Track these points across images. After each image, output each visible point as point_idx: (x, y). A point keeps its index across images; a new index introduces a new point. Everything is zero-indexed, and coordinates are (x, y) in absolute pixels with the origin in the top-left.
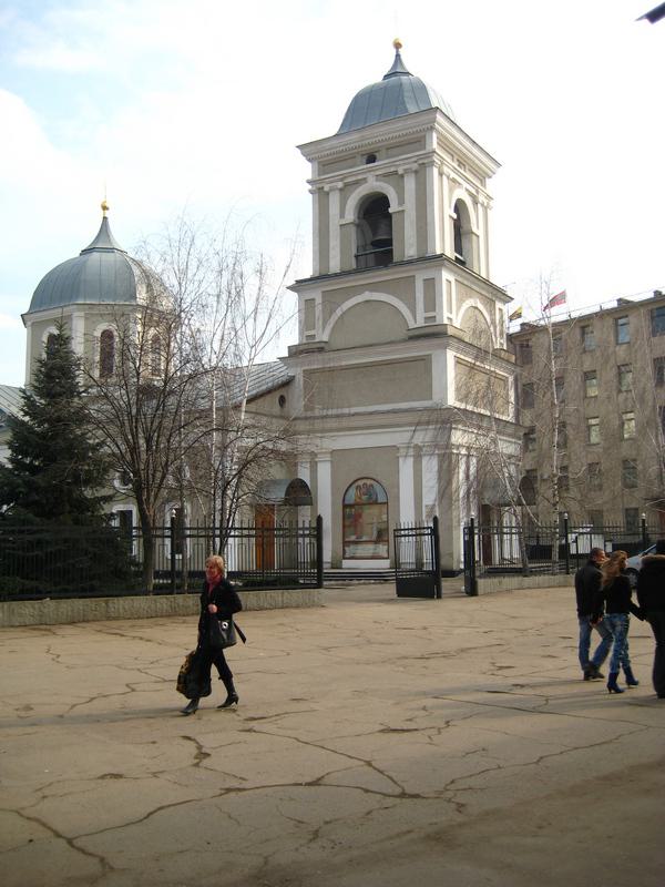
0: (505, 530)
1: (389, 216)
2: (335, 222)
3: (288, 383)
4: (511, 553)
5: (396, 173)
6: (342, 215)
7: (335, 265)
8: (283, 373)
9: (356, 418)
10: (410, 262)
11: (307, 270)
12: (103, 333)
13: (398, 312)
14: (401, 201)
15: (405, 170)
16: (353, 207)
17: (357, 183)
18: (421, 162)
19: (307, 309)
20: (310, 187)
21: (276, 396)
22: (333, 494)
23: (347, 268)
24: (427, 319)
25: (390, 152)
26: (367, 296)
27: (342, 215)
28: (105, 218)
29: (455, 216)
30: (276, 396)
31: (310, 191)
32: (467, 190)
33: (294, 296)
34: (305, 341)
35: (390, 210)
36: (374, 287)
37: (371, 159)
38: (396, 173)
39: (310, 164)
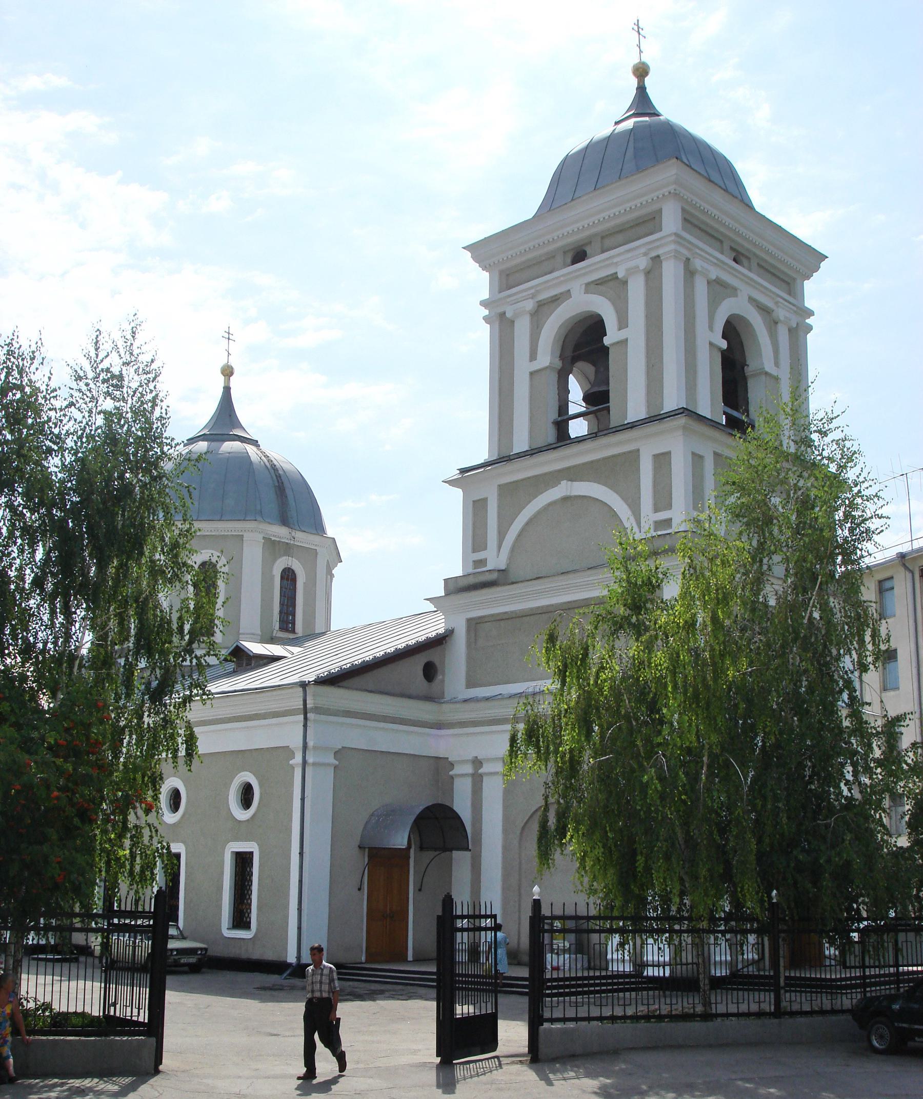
0: (459, 924)
1: (605, 350)
2: (523, 368)
3: (439, 642)
4: (681, 960)
5: (614, 277)
6: (533, 357)
7: (521, 443)
8: (435, 627)
9: (472, 705)
10: (632, 426)
11: (480, 453)
12: (203, 564)
13: (615, 515)
14: (623, 323)
15: (627, 270)
16: (551, 340)
17: (556, 300)
18: (653, 254)
19: (475, 514)
20: (486, 312)
21: (417, 665)
22: (505, 831)
23: (540, 443)
24: (659, 524)
25: (608, 242)
26: (563, 489)
27: (533, 357)
28: (227, 390)
29: (724, 345)
30: (417, 665)
31: (486, 319)
32: (751, 300)
33: (458, 493)
34: (471, 570)
35: (607, 341)
36: (573, 474)
37: (579, 256)
38: (614, 277)
39: (486, 275)
